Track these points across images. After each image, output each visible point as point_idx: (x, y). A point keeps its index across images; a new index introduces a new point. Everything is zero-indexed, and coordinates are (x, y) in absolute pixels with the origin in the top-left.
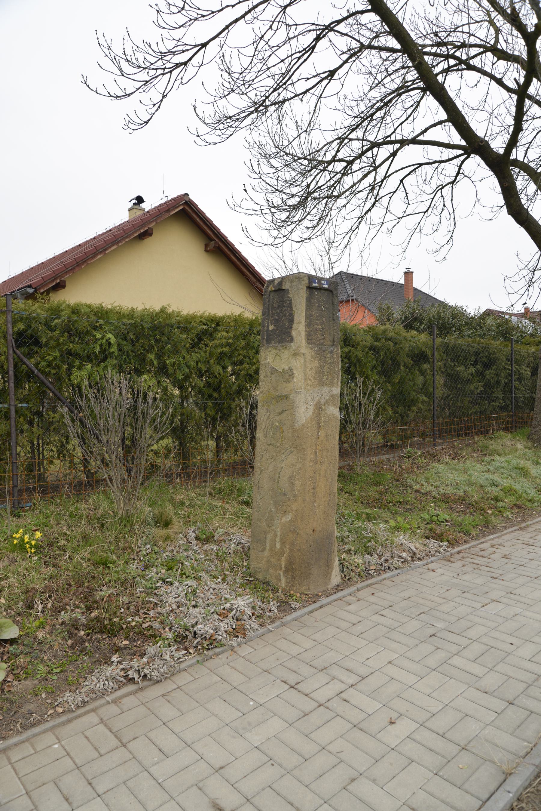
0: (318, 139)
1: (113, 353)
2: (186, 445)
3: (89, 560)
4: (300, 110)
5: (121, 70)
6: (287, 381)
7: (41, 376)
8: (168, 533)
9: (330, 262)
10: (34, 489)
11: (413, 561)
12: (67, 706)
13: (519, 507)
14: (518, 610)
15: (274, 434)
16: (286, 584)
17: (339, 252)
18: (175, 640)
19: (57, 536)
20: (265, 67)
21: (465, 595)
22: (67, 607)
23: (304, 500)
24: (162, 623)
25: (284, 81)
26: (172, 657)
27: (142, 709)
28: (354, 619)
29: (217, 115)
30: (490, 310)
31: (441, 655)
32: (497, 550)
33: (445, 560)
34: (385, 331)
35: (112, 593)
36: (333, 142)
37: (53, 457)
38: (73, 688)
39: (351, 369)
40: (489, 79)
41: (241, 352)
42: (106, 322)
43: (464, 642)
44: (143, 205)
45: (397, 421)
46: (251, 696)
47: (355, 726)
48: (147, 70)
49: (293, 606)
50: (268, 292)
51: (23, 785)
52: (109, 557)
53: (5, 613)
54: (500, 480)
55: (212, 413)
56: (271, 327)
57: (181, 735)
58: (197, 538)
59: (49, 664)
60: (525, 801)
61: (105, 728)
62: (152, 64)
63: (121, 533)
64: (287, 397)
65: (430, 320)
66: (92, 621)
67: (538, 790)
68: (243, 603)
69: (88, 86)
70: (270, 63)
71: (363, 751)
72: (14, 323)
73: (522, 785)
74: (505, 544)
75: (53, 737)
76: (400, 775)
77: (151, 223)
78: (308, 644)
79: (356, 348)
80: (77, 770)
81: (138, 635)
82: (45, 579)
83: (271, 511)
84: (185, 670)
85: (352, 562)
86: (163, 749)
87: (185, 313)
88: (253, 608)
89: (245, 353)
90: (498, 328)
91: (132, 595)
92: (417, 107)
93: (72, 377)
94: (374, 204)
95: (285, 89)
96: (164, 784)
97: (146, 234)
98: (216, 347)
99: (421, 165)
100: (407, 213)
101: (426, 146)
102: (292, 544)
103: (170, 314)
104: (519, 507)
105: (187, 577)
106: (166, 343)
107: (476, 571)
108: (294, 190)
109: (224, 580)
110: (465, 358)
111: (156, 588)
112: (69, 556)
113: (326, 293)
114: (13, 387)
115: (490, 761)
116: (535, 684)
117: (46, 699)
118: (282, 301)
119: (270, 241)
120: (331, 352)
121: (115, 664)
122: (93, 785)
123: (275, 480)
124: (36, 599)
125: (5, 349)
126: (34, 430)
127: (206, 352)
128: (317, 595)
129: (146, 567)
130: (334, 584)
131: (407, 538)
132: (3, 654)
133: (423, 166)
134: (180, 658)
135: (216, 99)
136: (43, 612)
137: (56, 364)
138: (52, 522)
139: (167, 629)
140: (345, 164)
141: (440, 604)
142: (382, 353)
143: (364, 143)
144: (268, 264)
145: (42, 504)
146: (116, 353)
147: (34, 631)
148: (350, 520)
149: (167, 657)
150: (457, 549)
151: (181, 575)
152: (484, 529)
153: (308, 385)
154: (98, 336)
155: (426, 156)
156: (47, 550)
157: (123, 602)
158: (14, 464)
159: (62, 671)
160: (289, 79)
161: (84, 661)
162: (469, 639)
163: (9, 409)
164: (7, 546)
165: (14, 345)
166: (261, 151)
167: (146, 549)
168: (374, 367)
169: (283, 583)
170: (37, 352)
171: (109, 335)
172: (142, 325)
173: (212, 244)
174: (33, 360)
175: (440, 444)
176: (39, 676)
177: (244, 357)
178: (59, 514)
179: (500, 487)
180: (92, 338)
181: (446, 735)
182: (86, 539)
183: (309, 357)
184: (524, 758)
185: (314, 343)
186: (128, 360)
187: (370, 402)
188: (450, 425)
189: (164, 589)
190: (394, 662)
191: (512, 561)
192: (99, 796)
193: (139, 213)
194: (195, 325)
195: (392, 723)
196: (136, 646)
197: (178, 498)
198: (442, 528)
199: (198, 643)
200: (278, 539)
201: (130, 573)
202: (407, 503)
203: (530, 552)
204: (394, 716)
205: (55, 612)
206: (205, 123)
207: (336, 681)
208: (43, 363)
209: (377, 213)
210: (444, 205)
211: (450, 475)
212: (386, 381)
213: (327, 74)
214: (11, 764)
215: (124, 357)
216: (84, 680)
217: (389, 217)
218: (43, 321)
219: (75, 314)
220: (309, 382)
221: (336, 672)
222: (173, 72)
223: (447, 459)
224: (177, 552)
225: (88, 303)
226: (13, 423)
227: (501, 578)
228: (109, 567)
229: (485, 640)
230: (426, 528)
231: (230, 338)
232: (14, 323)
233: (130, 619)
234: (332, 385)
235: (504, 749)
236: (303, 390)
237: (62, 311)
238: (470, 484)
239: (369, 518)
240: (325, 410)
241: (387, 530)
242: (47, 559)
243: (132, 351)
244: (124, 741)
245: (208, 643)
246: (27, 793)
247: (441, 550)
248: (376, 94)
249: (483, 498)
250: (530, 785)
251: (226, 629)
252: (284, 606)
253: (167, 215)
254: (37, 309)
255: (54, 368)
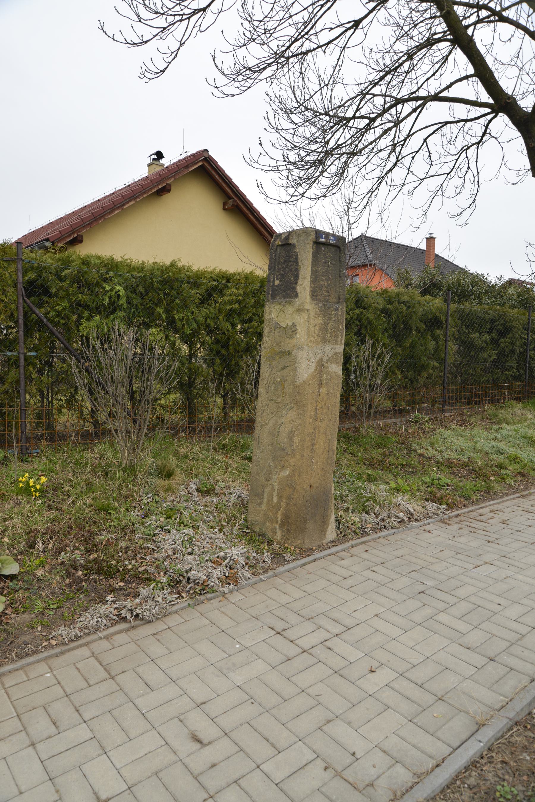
0: (341, 94)
1: (122, 305)
2: (193, 401)
3: (91, 506)
4: (322, 62)
5: (138, 16)
6: (290, 337)
7: (50, 326)
8: (169, 484)
9: (349, 224)
10: (42, 436)
11: (410, 522)
12: (61, 639)
13: (523, 475)
14: (510, 573)
15: (275, 390)
16: (282, 536)
17: (357, 213)
18: (169, 584)
19: (62, 482)
20: (287, 15)
21: (459, 556)
22: (67, 548)
23: (302, 456)
24: (157, 567)
25: (306, 30)
26: (164, 599)
27: (133, 646)
28: (346, 573)
29: (238, 66)
30: (512, 279)
31: (428, 611)
32: (495, 516)
33: (443, 522)
34: (398, 294)
35: (112, 538)
36: (356, 97)
37: (61, 406)
38: (68, 623)
39: (358, 328)
40: (523, 33)
41: (251, 309)
42: (115, 275)
43: (452, 600)
44: (162, 161)
45: (406, 386)
46: (237, 639)
47: (336, 672)
48: (165, 17)
49: (286, 558)
50: (275, 247)
51: (14, 708)
52: (110, 504)
53: (7, 551)
54: (506, 448)
55: (219, 369)
56: (277, 282)
57: (167, 671)
58: (198, 490)
59: (47, 600)
60: (496, 751)
61: (96, 661)
62: (170, 9)
63: (124, 482)
64: (289, 353)
65: (449, 287)
66: (90, 563)
67: (509, 742)
68: (237, 552)
69: (105, 32)
70: (293, 11)
71: (342, 696)
72: (25, 273)
73: (493, 736)
74: (504, 510)
75: (46, 667)
76: (375, 719)
77: (169, 178)
78: (297, 594)
79: (368, 310)
80: (66, 698)
81: (133, 577)
82: (47, 522)
83: (270, 466)
84: (177, 612)
85: (348, 519)
86: (149, 683)
87: (195, 268)
88: (248, 558)
89: (254, 310)
90: (519, 296)
91: (131, 540)
92: (445, 61)
93: (81, 328)
94: (395, 164)
95: (307, 39)
96: (147, 715)
97: (165, 190)
98: (226, 303)
99: (446, 123)
100: (430, 174)
101: (452, 104)
102: (289, 498)
103: (180, 268)
104: (523, 475)
105: (185, 526)
106: (175, 298)
107: (472, 534)
108: (313, 147)
109: (221, 530)
110: (481, 326)
111: (154, 535)
112: (73, 502)
113: (333, 249)
114: (22, 335)
115: (464, 712)
116: (518, 643)
117: (41, 631)
118: (289, 256)
119: (288, 198)
120: (336, 309)
121: (109, 603)
122: (80, 712)
123: (274, 435)
124: (38, 540)
125: (15, 298)
126: (42, 378)
127: (215, 308)
128: (312, 549)
129: (146, 515)
130: (329, 540)
131: (405, 499)
132: (3, 588)
133: (449, 125)
134: (173, 601)
135: (235, 48)
136: (44, 552)
137: (65, 314)
138: (58, 469)
139: (162, 574)
140: (367, 121)
141: (433, 564)
142: (394, 316)
143: (388, 99)
144: (281, 218)
145: (49, 451)
146: (125, 306)
147: (35, 570)
148: (351, 480)
149: (159, 599)
150: (455, 513)
151: (180, 523)
152: (485, 495)
153: (311, 341)
154: (108, 287)
155: (452, 114)
156: (52, 495)
157: (121, 547)
158: (23, 411)
159: (58, 607)
160: (311, 28)
161: (80, 599)
162: (457, 597)
163: (19, 357)
164: (13, 489)
165: (24, 294)
166: (281, 106)
167: (148, 498)
168: (386, 330)
169: (279, 536)
170: (47, 302)
171: (118, 288)
172: (151, 279)
173: (230, 203)
174: (42, 310)
175: (449, 411)
176: (36, 611)
177: (254, 314)
178: (66, 462)
179: (505, 455)
180: (101, 290)
181: (424, 686)
182: (89, 486)
183: (313, 313)
184: (499, 711)
185: (319, 300)
186: (137, 313)
187: (379, 365)
188: (460, 392)
189: (162, 536)
190: (381, 616)
191: (510, 527)
192: (85, 722)
193: (158, 169)
194: (205, 281)
195: (373, 671)
196: (131, 588)
197: (183, 451)
198: (442, 492)
199: (190, 588)
200: (275, 493)
201: (130, 520)
202: (410, 466)
203: (529, 519)
204: (375, 665)
205: (55, 552)
206: (224, 74)
207: (321, 630)
208: (53, 313)
209: (399, 174)
210: (469, 167)
211: (455, 441)
212: (396, 345)
213: (352, 24)
214: (4, 688)
215: (133, 310)
216: (79, 616)
217: (410, 178)
218: (53, 270)
219: (86, 265)
220: (312, 339)
221: (323, 621)
222: (191, 19)
223: (454, 425)
224: (177, 502)
225: (99, 254)
226: (22, 371)
227: (497, 542)
228: (110, 513)
229: (473, 599)
230: (426, 491)
231: (240, 295)
232: (25, 273)
233: (126, 563)
234: (336, 343)
235: (480, 702)
236: (306, 347)
237: (73, 261)
238: (475, 450)
239: (370, 479)
240: (327, 367)
241: (386, 490)
242: (51, 503)
243: (141, 305)
244: (113, 674)
245: (200, 588)
246: (18, 716)
247: (439, 512)
248: (402, 47)
249: (487, 464)
250: (502, 736)
251: (219, 576)
252: (278, 558)
253: (186, 171)
254: (50, 260)
255: (62, 318)
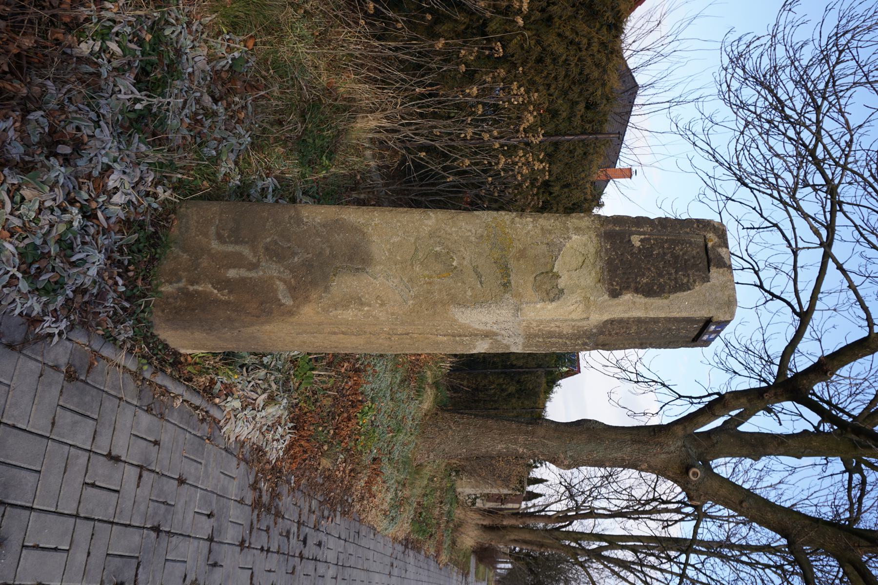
6: (537, 288)
83: (294, 254)
200: (243, 273)
